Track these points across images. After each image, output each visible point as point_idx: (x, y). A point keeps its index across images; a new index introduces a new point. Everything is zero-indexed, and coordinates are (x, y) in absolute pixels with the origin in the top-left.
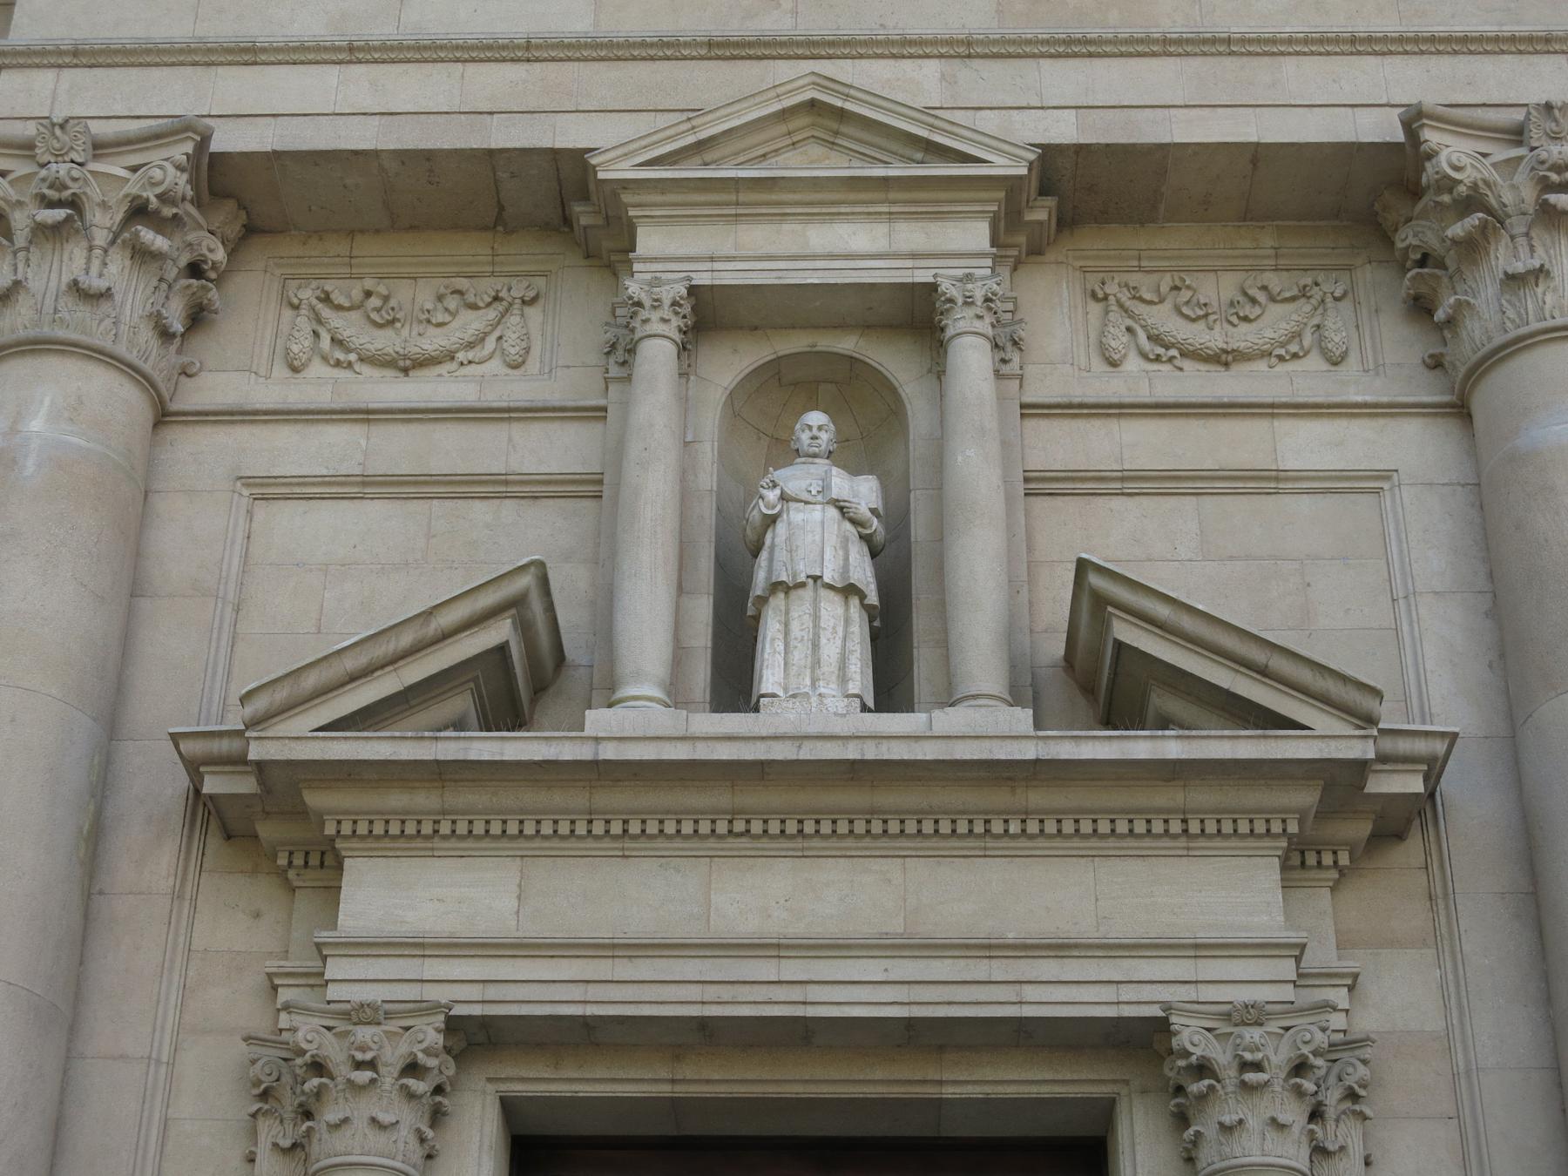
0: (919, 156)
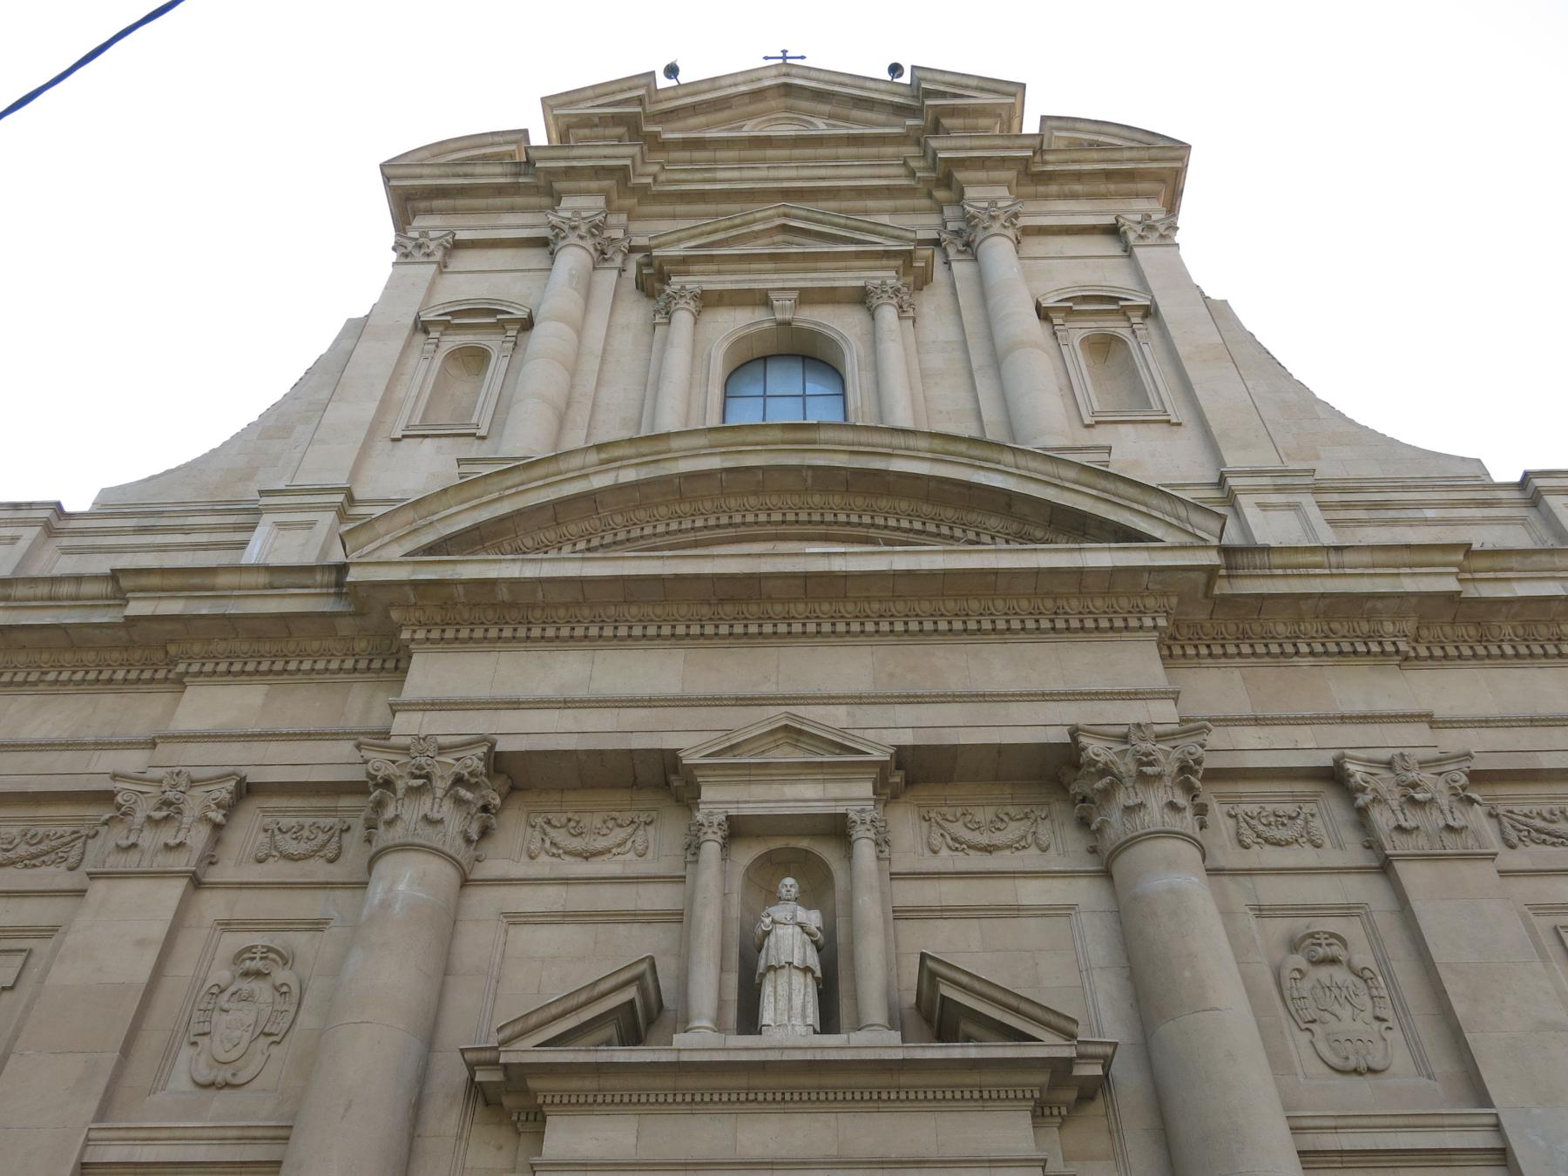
0: (838, 751)
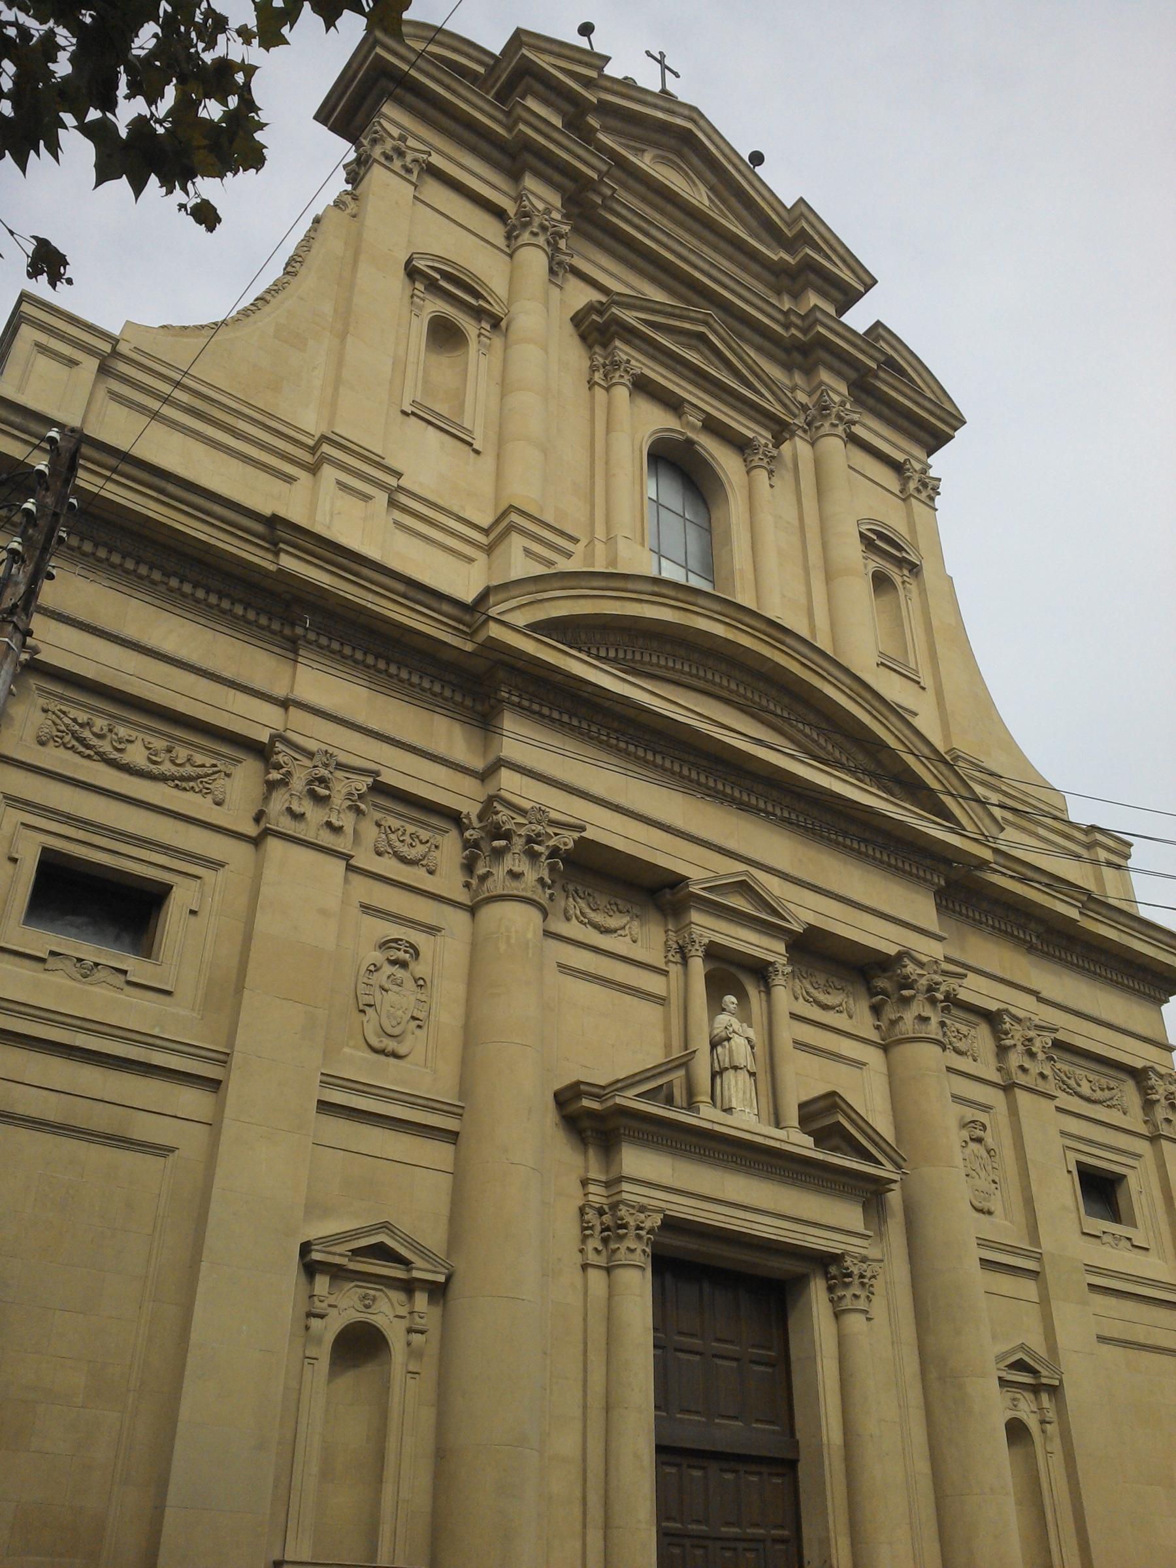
0: (769, 911)
